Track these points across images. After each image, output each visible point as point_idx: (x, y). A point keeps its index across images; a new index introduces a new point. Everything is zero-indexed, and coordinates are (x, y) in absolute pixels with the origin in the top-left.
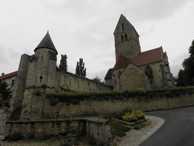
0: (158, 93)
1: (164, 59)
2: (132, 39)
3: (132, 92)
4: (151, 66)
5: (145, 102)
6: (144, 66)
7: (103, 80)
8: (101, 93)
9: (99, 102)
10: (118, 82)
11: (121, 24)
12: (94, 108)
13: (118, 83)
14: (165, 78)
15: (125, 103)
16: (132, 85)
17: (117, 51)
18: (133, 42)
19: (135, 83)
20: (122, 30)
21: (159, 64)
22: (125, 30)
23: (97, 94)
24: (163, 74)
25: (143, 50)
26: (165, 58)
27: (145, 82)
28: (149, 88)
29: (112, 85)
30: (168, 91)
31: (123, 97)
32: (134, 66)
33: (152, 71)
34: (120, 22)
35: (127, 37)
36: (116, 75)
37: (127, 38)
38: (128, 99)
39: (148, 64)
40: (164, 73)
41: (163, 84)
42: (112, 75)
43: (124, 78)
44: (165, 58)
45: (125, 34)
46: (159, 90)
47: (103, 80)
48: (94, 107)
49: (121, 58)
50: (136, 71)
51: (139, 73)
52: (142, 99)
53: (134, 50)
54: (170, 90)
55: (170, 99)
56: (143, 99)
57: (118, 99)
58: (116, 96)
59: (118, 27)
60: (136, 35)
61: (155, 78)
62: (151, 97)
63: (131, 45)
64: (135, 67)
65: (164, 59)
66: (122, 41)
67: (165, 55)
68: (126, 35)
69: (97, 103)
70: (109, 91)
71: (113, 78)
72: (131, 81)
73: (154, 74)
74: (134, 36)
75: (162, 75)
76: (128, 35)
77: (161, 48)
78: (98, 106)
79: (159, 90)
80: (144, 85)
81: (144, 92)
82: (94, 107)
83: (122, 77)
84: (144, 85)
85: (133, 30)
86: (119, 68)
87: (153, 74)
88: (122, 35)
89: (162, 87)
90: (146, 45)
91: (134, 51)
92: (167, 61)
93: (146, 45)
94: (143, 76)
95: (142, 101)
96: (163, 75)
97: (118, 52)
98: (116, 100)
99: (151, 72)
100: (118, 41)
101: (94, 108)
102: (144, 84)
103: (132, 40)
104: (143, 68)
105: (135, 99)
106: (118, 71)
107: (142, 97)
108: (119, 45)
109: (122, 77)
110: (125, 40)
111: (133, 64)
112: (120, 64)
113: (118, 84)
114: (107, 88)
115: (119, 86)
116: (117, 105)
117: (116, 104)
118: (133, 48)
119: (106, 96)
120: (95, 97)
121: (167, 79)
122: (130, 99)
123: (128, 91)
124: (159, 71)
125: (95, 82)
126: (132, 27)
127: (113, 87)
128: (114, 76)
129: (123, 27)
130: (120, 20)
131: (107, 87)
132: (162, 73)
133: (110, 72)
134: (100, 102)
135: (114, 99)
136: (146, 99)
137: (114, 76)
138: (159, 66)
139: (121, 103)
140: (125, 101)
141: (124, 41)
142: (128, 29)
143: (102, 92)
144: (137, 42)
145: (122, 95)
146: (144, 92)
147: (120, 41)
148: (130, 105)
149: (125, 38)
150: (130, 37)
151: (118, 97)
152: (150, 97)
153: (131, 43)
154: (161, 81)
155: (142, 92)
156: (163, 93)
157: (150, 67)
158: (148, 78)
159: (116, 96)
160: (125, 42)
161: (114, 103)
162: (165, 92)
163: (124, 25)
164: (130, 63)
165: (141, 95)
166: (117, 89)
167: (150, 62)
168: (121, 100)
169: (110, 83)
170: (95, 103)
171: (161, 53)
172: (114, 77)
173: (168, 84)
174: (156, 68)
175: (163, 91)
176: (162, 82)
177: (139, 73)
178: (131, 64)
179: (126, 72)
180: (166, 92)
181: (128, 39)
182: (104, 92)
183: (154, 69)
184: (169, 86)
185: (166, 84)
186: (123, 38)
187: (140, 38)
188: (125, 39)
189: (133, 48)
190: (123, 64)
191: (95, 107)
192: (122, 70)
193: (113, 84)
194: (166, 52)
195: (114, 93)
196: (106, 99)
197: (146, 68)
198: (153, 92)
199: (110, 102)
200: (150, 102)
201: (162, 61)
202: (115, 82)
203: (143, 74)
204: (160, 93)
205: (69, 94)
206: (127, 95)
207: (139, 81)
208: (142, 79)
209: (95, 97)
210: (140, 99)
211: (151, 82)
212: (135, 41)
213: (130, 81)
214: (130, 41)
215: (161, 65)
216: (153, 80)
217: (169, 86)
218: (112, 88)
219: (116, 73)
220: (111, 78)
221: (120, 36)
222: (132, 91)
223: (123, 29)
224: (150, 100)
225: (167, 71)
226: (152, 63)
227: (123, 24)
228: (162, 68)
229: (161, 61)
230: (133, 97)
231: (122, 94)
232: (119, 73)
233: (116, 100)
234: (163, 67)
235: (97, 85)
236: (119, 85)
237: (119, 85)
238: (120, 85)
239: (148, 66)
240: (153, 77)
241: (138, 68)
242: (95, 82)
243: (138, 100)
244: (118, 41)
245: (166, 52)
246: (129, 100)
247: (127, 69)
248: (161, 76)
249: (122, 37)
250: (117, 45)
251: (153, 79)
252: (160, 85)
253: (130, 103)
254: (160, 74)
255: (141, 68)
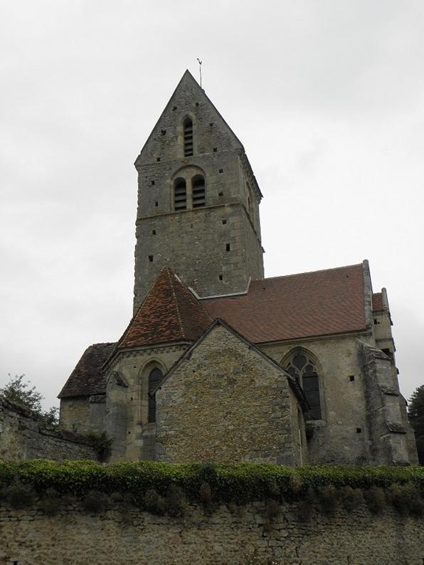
0: (359, 490)
1: (376, 323)
2: (231, 205)
3: (233, 477)
4: (315, 349)
5: (296, 531)
6: (281, 348)
7: (49, 403)
8: (68, 469)
9: (46, 523)
10: (136, 420)
11: (180, 119)
12: (17, 554)
13: (140, 424)
14: (379, 419)
15: (191, 535)
16: (217, 442)
17: (144, 256)
18: (231, 220)
19: (233, 430)
20: (182, 150)
21: (351, 346)
22: (195, 152)
23: (40, 474)
24: (367, 396)
25: (274, 267)
26: (379, 318)
27: (288, 430)
28: (295, 465)
29: (104, 435)
30: (403, 482)
31: (184, 503)
32: (233, 342)
33: (315, 376)
34: (175, 108)
35: (203, 191)
36: (131, 382)
37: (203, 198)
38: (209, 513)
39: (301, 342)
40: (373, 393)
41: (368, 448)
42: (109, 378)
43: (178, 398)
44: (379, 318)
45: (194, 172)
46: (364, 477)
47: (49, 403)
48: (15, 548)
49: (168, 293)
50: (246, 368)
51: (258, 383)
52: (281, 519)
53: (234, 259)
54: (412, 478)
55: (410, 524)
56: (289, 516)
57: (155, 511)
58: (151, 493)
59: (164, 133)
60: (247, 190)
61: (332, 413)
62: (327, 508)
63: (223, 235)
64: (242, 347)
65: (376, 323)
66: (177, 209)
67: (379, 305)
68: (199, 182)
69: (34, 524)
70: (79, 464)
71: (114, 395)
72: (214, 415)
73: (327, 394)
74: (243, 194)
75: (362, 405)
76: (210, 180)
77: (361, 272)
78: (39, 546)
79: (364, 477)
80: (282, 446)
81: (297, 481)
82: (15, 548)
83: (169, 396)
84: (282, 446)
85: (240, 161)
86: (153, 345)
87: (321, 391)
88: (178, 176)
89: (362, 459)
90: (294, 240)
91: (236, 264)
92: (388, 337)
93: (294, 240)
94: (279, 400)
95: (281, 526)
96: (368, 402)
97: (151, 258)
98: (147, 517)
99: (313, 378)
100: (157, 205)
101: (17, 554)
102: (282, 438)
103: (228, 210)
104: (278, 354)
105: (249, 517)
106: (143, 359)
107: (284, 509)
108: (156, 222)
109: (169, 396)
110: (195, 206)
111: (234, 332)
112: (157, 324)
113: (138, 430)
114: (77, 448)
115: (140, 443)
116: (147, 543)
117: (142, 538)
118: (228, 249)
119: (92, 492)
120: (27, 489)
121: (384, 424)
122: (222, 516)
123: (217, 467)
124: (352, 378)
125: (15, 409)
126: (235, 146)
127: (109, 443)
128: (121, 383)
129: (186, 139)
130: (176, 98)
131: (77, 443)
132: (366, 392)
133: (96, 368)
134: (53, 521)
135: (138, 510)
136: (302, 520)
137: (121, 383)
138: (354, 358)
139: (172, 533)
140: (194, 523)
141: (185, 207)
142: (215, 150)
143: (49, 464)
144: (253, 227)
145: (180, 489)
146: (297, 481)
147: (168, 204)
148: (217, 548)
149: (194, 192)
150: (221, 194)
151: (161, 499)
152: (320, 508)
153: (224, 222)
154: (359, 431)
155: (286, 479)
156: (380, 491)
157: (312, 354)
158: (299, 411)
159: (151, 493)
160: (191, 215)
161: (131, 529)
162: (390, 485)
163: (194, 128)
164: (219, 324)
165: (278, 493)
166: (128, 455)
167: (310, 331)
168: (173, 516)
169: (87, 421)
170: (24, 525)
171: (363, 293)
172: (121, 387)
173: (389, 451)
174: (336, 364)
175: (382, 483)
176: (362, 439)
177: (258, 383)
178: (220, 329)
179: (190, 365)
180: (394, 485)
181: (210, 203)
182: (86, 468)
183: (325, 370)
184: (396, 458)
185: (379, 446)
186: (185, 194)
187: (266, 210)
188: (195, 199)
189: (228, 249)
190: (177, 327)
191: (24, 552)
192: (167, 357)
193: (109, 428)
194: (384, 290)
195: (136, 472)
196: (93, 509)
197: (291, 359)
198: (338, 484)
199: (111, 525)
200: (319, 537)
201: (371, 334)
202: (124, 419)
203: (281, 385)
204: (366, 492)
205: (300, 408)
206: (206, 489)
207: (256, 422)
208: (274, 411)
209: (27, 489)
210: (272, 515)
211: (310, 434)
212: (244, 216)
213: (211, 420)
214: (219, 212)
215: (362, 354)
216: (317, 422)
217: (396, 458)
218: (101, 448)
219: (130, 368)
220: (101, 397)
221: (170, 182)
222: (235, 473)
223: (186, 145)
224: (320, 527)
225: (389, 386)
226: (322, 338)
227: (188, 123)
228: (364, 368)
229: (364, 332)
230: (238, 505)
231: (181, 483)
232: (149, 370)
233: (145, 514)
234: (373, 363)
235: (23, 428)
236: (140, 437)
237: (140, 437)
238: (145, 438)
239: (299, 349)
240: (322, 404)
241: (254, 355)
242: (14, 405)
243: (259, 520)
244: (157, 205)
245: (384, 290)
246: (216, 519)
247: (199, 352)
248: (360, 407)
249: (180, 184)
250: (147, 223)
251: (318, 417)
252: (350, 451)
253: (217, 533)
254: (354, 393)
255: (266, 351)
